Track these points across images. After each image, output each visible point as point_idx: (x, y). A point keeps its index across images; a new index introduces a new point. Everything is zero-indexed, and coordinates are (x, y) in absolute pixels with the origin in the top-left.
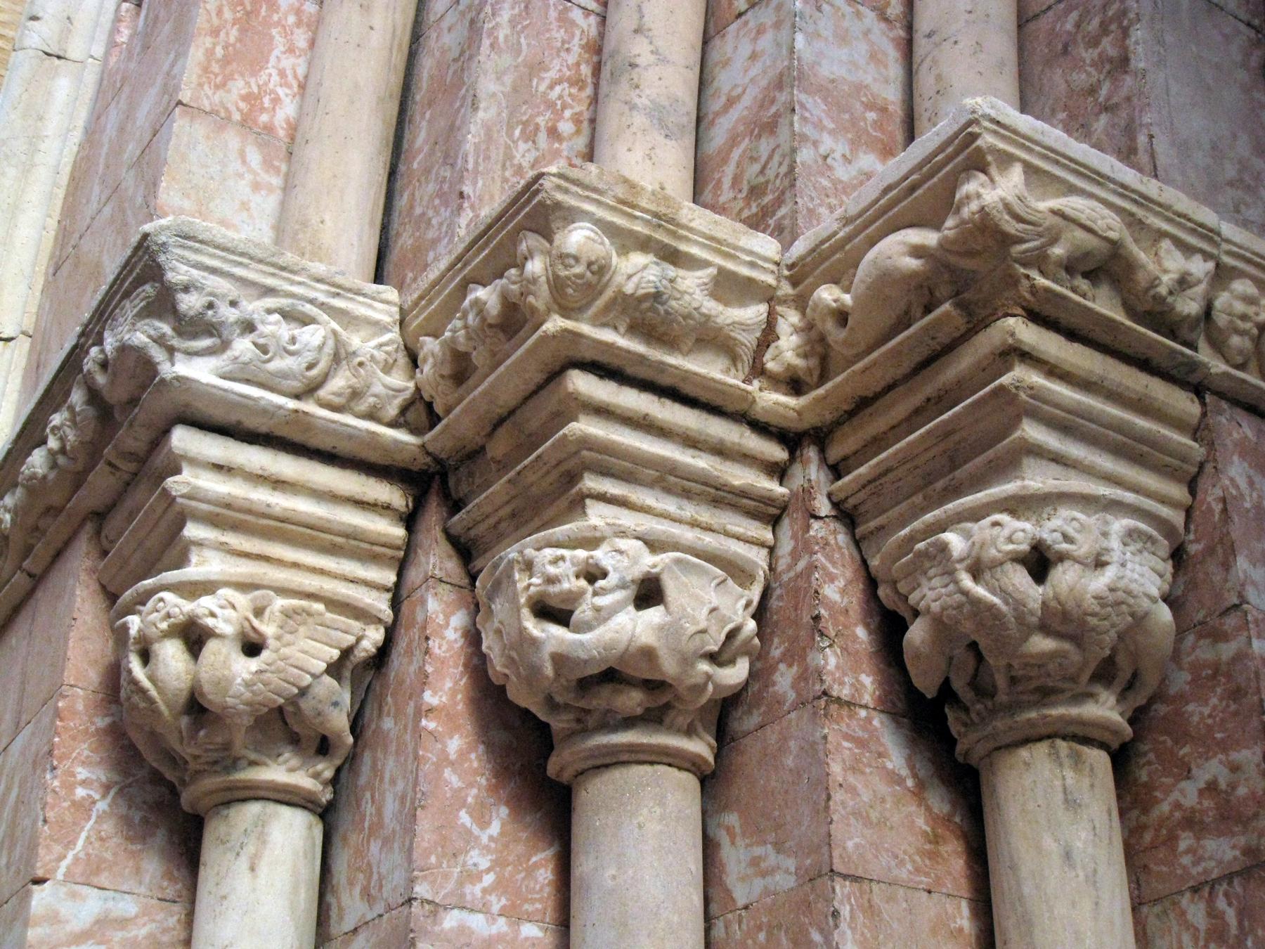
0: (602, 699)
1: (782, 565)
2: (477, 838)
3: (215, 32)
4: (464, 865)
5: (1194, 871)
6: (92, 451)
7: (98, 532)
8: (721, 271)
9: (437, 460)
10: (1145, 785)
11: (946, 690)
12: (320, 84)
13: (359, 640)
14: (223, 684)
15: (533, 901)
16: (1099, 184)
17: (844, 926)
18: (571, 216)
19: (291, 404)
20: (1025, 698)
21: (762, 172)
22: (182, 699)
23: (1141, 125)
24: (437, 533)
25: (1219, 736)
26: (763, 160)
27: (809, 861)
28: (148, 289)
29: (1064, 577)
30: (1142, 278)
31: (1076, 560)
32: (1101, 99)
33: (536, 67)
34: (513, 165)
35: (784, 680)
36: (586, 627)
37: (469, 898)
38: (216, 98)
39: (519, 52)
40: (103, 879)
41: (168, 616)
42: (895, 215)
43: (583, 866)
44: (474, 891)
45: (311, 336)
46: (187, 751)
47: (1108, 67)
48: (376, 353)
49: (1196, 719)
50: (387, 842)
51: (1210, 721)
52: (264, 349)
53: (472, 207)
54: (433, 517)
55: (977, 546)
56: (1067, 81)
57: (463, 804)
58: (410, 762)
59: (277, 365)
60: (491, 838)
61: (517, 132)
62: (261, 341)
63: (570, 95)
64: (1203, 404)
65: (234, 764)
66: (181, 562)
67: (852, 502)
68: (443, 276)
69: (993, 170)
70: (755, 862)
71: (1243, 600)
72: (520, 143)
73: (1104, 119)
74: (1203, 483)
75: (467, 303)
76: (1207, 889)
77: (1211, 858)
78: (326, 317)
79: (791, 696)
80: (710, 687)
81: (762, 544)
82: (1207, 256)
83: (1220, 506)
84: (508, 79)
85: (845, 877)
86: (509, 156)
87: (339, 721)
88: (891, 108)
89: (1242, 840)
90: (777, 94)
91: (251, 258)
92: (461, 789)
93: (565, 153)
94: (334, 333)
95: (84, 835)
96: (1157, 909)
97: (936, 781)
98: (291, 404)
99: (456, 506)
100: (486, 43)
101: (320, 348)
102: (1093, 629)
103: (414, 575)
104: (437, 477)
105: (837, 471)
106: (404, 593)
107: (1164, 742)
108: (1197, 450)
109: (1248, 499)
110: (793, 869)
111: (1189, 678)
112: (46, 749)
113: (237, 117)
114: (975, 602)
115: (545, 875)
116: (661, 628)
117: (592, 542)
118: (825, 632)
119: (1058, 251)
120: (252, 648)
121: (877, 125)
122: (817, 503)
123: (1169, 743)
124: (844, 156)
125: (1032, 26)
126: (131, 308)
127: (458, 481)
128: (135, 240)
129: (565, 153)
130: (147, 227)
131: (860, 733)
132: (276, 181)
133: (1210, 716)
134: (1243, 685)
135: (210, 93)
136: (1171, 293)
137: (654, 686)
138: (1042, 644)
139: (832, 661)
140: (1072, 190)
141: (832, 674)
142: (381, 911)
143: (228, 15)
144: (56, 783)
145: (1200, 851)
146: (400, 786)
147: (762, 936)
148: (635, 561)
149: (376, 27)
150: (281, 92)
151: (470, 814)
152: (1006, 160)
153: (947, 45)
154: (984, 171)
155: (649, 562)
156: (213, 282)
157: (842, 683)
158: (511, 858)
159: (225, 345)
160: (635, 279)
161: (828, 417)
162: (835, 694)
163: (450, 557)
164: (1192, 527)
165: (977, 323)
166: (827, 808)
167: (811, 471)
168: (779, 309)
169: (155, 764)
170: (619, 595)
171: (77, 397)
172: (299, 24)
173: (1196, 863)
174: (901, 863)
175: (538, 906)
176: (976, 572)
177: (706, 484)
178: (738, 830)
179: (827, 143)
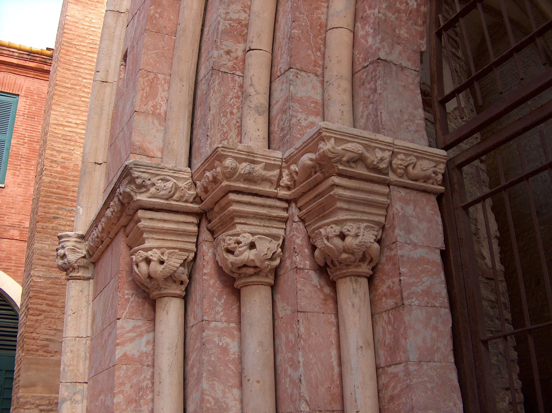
0: (244, 270)
2: (218, 304)
3: (143, 90)
6: (122, 212)
7: (125, 231)
8: (266, 163)
12: (171, 103)
13: (188, 257)
14: (156, 272)
15: (233, 318)
16: (356, 138)
17: (300, 324)
18: (226, 157)
19: (166, 202)
20: (343, 267)
22: (147, 276)
24: (206, 229)
26: (284, 121)
28: (128, 178)
29: (348, 240)
30: (369, 161)
31: (350, 236)
33: (225, 96)
35: (288, 263)
36: (238, 256)
38: (145, 108)
39: (221, 92)
40: (134, 317)
41: (141, 256)
42: (306, 149)
43: (243, 310)
44: (218, 317)
45: (169, 185)
46: (149, 286)
48: (186, 186)
50: (198, 305)
53: (210, 139)
54: (204, 224)
57: (215, 296)
59: (162, 193)
60: (222, 304)
61: (222, 115)
62: (157, 188)
63: (236, 101)
64: (390, 188)
65: (160, 288)
66: (143, 243)
68: (199, 167)
69: (326, 141)
70: (283, 307)
72: (223, 118)
73: (371, 105)
75: (205, 176)
78: (173, 179)
79: (290, 267)
80: (270, 267)
81: (283, 229)
82: (389, 150)
84: (218, 100)
85: (301, 312)
86: (220, 122)
87: (185, 278)
89: (395, 300)
91: (152, 167)
93: (235, 118)
94: (175, 183)
95: (128, 307)
96: (378, 315)
97: (326, 286)
98: (166, 202)
99: (210, 222)
100: (212, 91)
101: (172, 187)
102: (356, 252)
103: (201, 239)
105: (300, 209)
106: (199, 243)
112: (117, 286)
113: (151, 112)
114: (328, 246)
115: (236, 311)
116: (255, 255)
117: (238, 235)
119: (345, 159)
120: (162, 262)
122: (294, 219)
124: (305, 118)
125: (356, 75)
126: (125, 182)
128: (124, 165)
129: (235, 118)
130: (126, 163)
132: (162, 128)
135: (143, 107)
136: (378, 163)
137: (256, 267)
138: (344, 256)
139: (298, 259)
140: (349, 142)
141: (298, 262)
143: (146, 84)
144: (120, 295)
146: (200, 293)
147: (285, 325)
148: (248, 239)
149: (184, 85)
150: (162, 103)
152: (329, 138)
153: (331, 85)
154: (324, 141)
155: (251, 239)
157: (301, 264)
159: (148, 190)
160: (244, 170)
163: (208, 234)
165: (326, 178)
166: (296, 296)
167: (294, 210)
168: (283, 170)
169: (143, 289)
170: (245, 247)
171: (116, 199)
172: (165, 83)
174: (316, 307)
176: (328, 238)
177: (266, 216)
179: (300, 115)
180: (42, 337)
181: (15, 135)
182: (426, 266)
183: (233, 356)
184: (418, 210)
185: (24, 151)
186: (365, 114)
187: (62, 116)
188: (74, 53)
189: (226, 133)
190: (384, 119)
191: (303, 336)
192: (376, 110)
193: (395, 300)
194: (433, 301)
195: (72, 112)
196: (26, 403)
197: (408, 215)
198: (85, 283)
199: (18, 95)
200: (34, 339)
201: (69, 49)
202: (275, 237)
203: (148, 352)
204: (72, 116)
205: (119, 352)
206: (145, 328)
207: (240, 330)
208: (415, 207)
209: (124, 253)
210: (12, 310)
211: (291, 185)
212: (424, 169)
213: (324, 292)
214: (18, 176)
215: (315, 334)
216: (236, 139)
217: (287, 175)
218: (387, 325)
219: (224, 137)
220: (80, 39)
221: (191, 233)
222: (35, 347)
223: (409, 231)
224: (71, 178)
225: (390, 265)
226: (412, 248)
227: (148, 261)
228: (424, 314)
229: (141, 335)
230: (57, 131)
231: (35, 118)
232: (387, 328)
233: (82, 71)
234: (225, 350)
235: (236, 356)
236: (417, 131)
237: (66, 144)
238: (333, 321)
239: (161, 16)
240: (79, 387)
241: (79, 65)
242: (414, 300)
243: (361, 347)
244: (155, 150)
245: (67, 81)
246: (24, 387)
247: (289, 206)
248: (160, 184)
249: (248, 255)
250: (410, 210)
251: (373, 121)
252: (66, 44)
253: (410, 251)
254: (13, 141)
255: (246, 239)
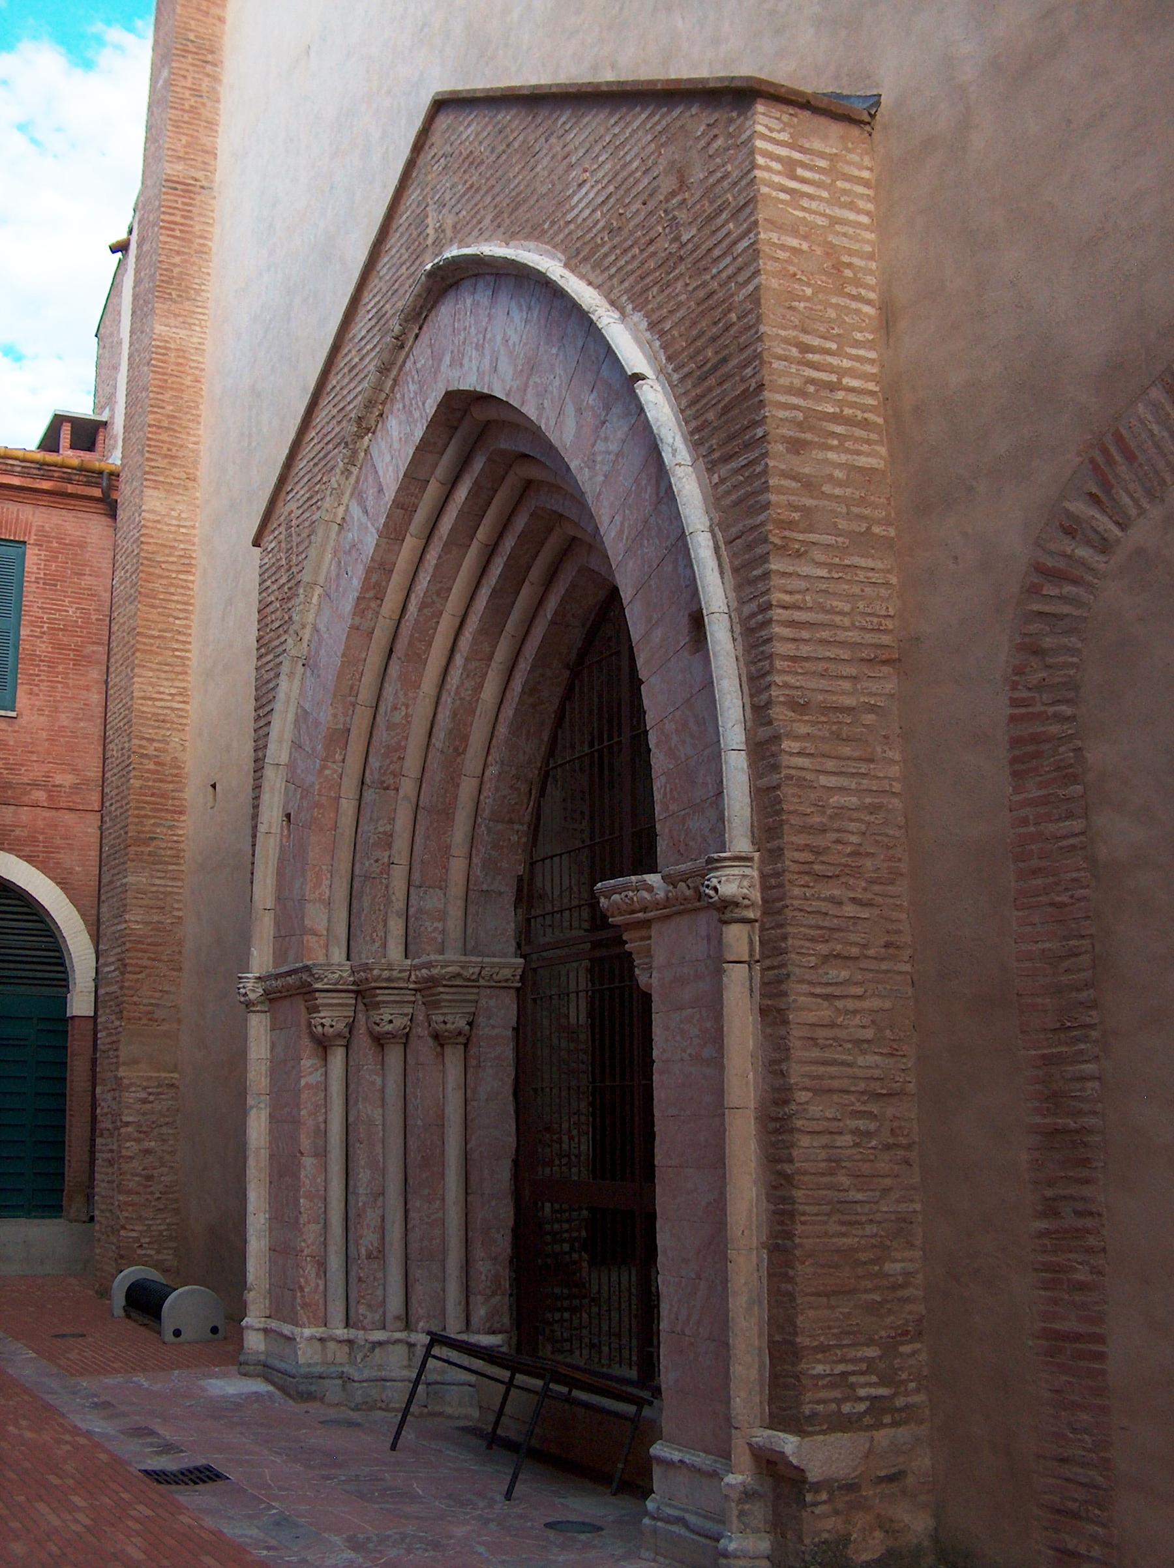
29: (448, 1026)
35: (414, 1031)
54: (359, 998)
120: (332, 1026)
155: (390, 1018)
167: (419, 996)
180: (145, 1001)
181: (25, 619)
185: (43, 647)
187: (151, 684)
188: (161, 577)
195: (163, 675)
196: (131, 1085)
198: (263, 1015)
199: (24, 543)
200: (135, 1004)
201: (151, 570)
202: (406, 1015)
204: (165, 683)
205: (303, 1082)
207: (383, 1069)
210: (41, 922)
214: (37, 695)
220: (167, 551)
222: (137, 1014)
223: (489, 1018)
224: (170, 779)
227: (323, 1025)
229: (317, 1070)
230: (145, 709)
231: (55, 585)
233: (173, 606)
234: (373, 1083)
237: (159, 728)
239: (323, 816)
240: (263, 1098)
241: (168, 597)
245: (153, 625)
246: (124, 1064)
248: (330, 976)
249: (389, 1027)
252: (145, 562)
254: (22, 633)
255: (387, 1017)
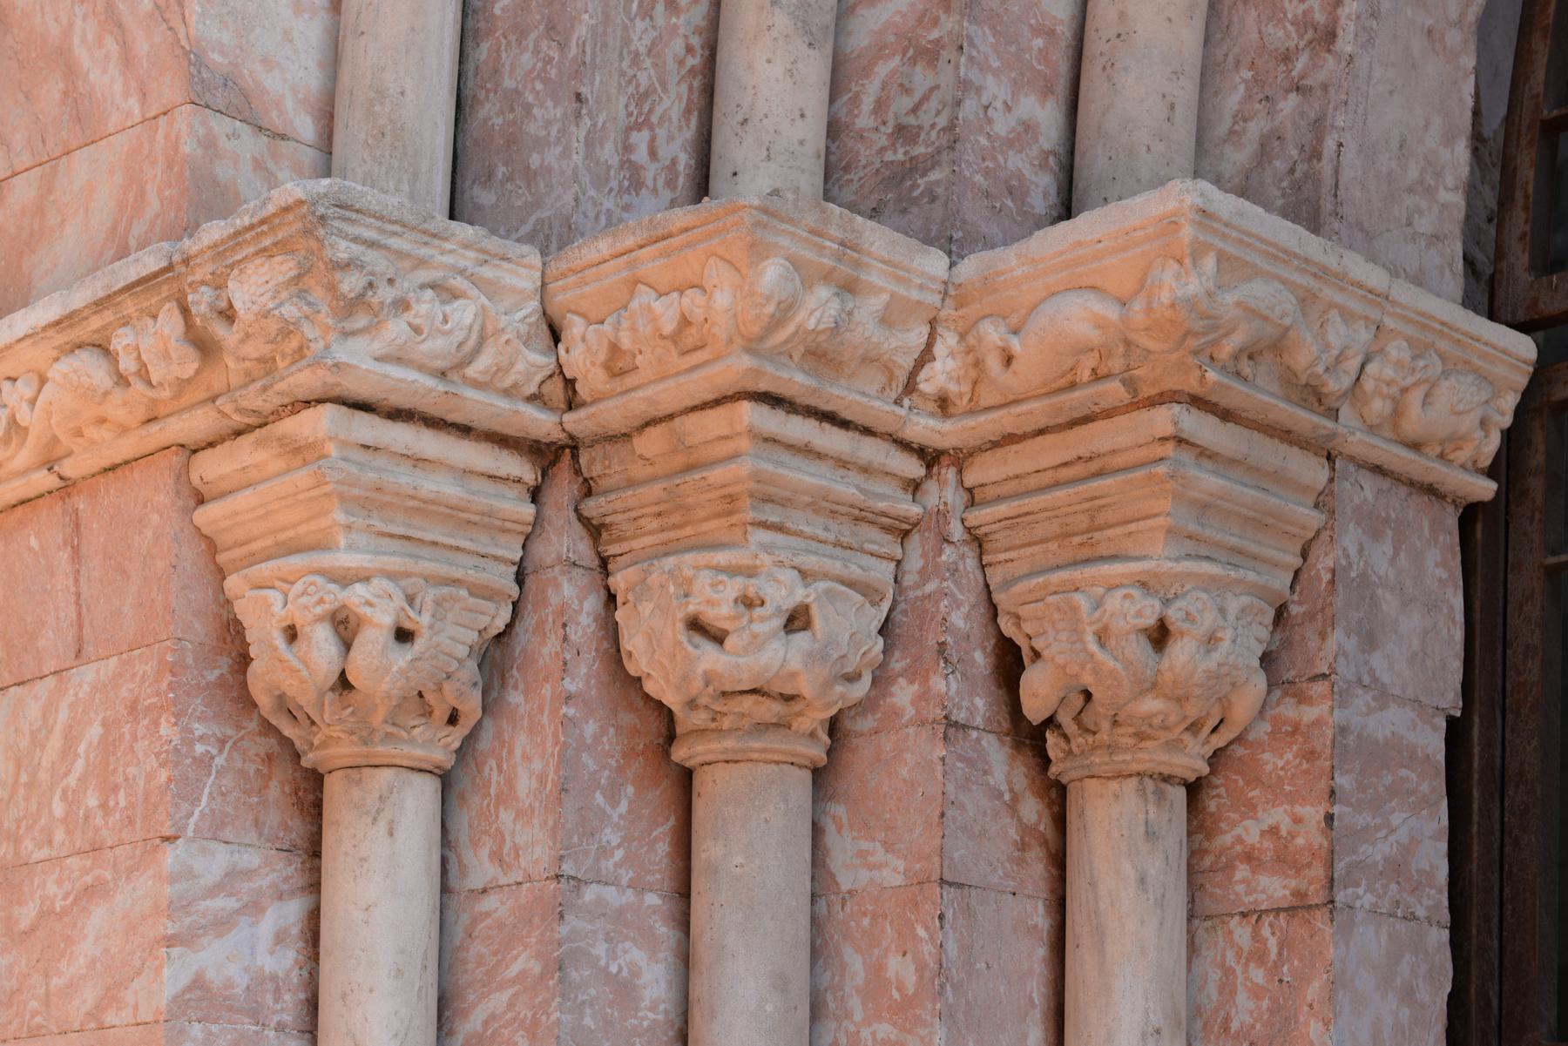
1: (909, 580)
2: (610, 817)
4: (600, 842)
5: (1246, 900)
8: (893, 295)
9: (571, 437)
10: (1212, 815)
11: (1050, 722)
17: (947, 926)
21: (915, 110)
23: (1332, 126)
25: (1288, 788)
26: (917, 96)
27: (918, 866)
32: (1294, 73)
34: (630, 52)
37: (604, 872)
41: (321, 601)
44: (608, 865)
47: (1310, 34)
49: (1269, 767)
51: (1282, 773)
52: (417, 330)
53: (590, 114)
55: (1108, 614)
56: (1260, 32)
58: (549, 744)
60: (620, 816)
62: (417, 321)
67: (983, 530)
71: (1334, 671)
73: (1293, 99)
74: (1317, 551)
76: (1255, 917)
77: (1263, 892)
79: (910, 712)
83: (1329, 576)
85: (951, 884)
86: (626, 42)
88: (1059, 29)
89: (1293, 883)
90: (943, 17)
92: (596, 771)
93: (682, 31)
94: (483, 307)
95: (207, 791)
101: (470, 328)
103: (539, 550)
104: (568, 451)
107: (1237, 781)
108: (1315, 519)
109: (1355, 567)
110: (901, 869)
111: (1269, 730)
117: (751, 572)
118: (950, 659)
120: (403, 636)
121: (1043, 55)
123: (1241, 783)
124: (1005, 103)
127: (592, 461)
129: (682, 31)
131: (971, 754)
133: (1282, 768)
134: (1318, 750)
142: (520, 879)
145: (1254, 884)
147: (866, 922)
148: (791, 592)
151: (603, 794)
155: (800, 594)
156: (370, 256)
158: (636, 834)
160: (818, 314)
161: (972, 443)
162: (953, 718)
163: (582, 538)
164: (1298, 588)
173: (1248, 894)
175: (658, 876)
178: (845, 821)
182: (1403, 772)
183: (651, 1016)
184: (1403, 560)
186: (1255, 128)
189: (646, 94)
190: (1347, 175)
191: (954, 971)
192: (1319, 126)
193: (1293, 883)
194: (1411, 900)
197: (1374, 578)
203: (281, 974)
206: (271, 877)
208: (1396, 549)
209: (187, 565)
211: (961, 395)
212: (1461, 407)
213: (1020, 820)
215: (988, 967)
216: (680, 129)
217: (952, 354)
218: (1246, 965)
219: (640, 114)
221: (508, 525)
225: (1289, 756)
226: (1373, 704)
228: (1384, 939)
229: (254, 908)
232: (1245, 971)
234: (625, 990)
235: (660, 1017)
236: (1437, 238)
238: (1040, 926)
242: (1360, 891)
243: (1158, 1032)
244: (289, 103)
247: (929, 475)
248: (426, 306)
250: (1380, 558)
251: (1292, 171)
253: (1367, 715)
